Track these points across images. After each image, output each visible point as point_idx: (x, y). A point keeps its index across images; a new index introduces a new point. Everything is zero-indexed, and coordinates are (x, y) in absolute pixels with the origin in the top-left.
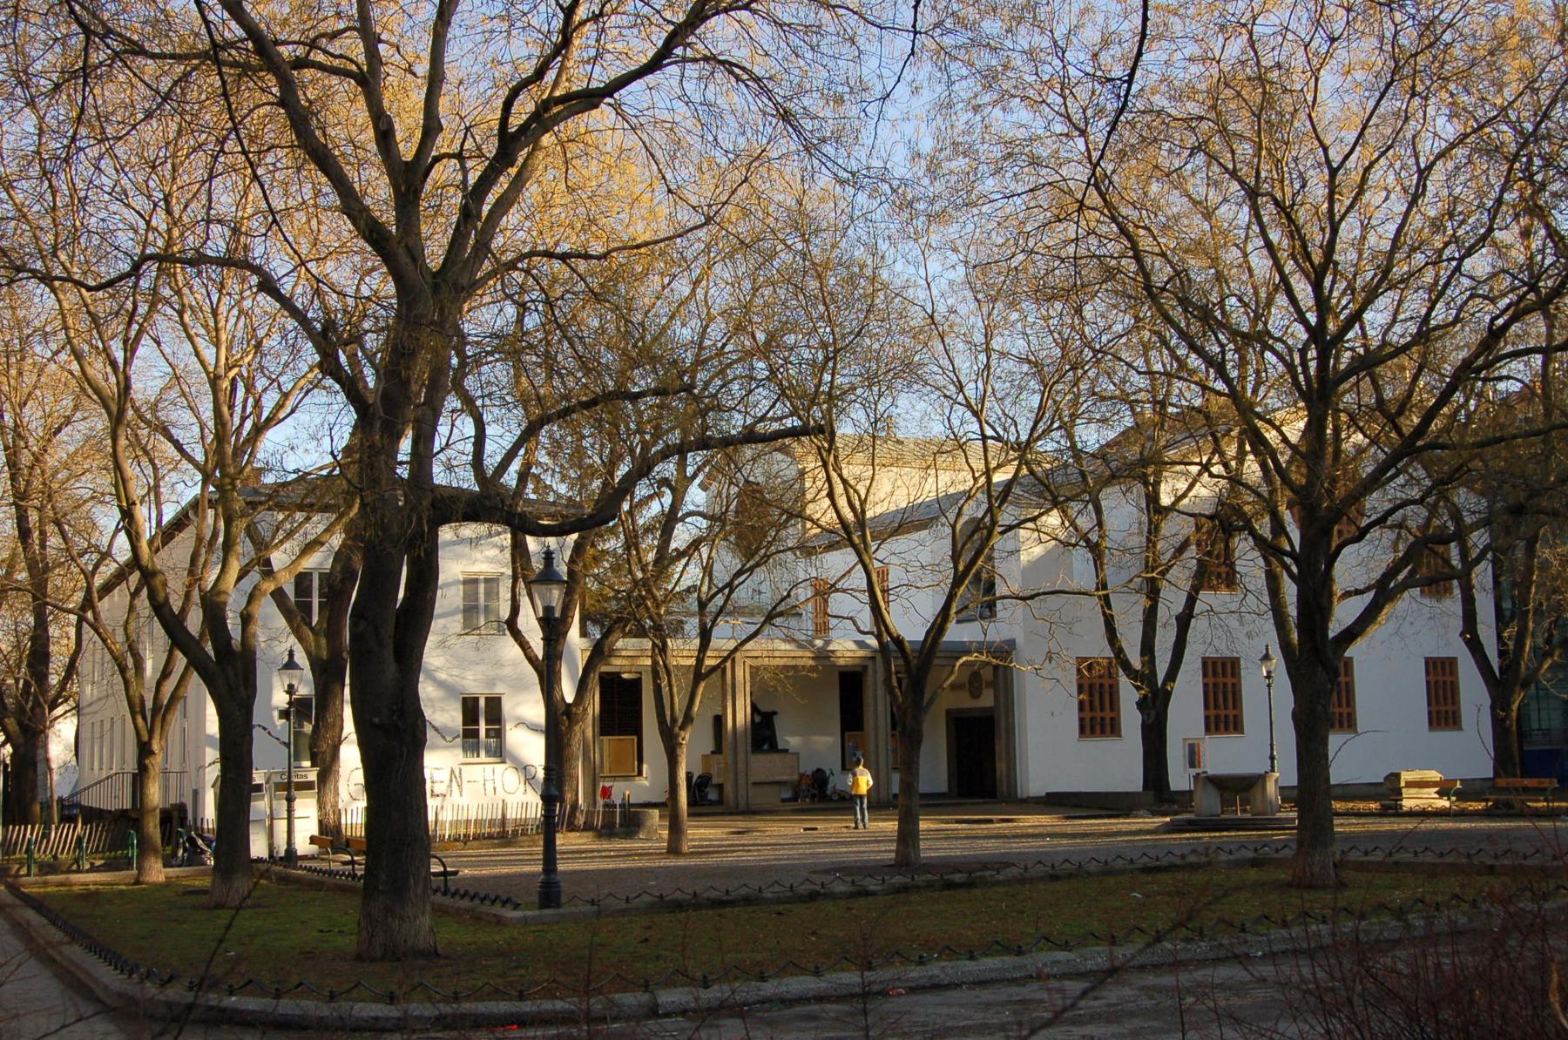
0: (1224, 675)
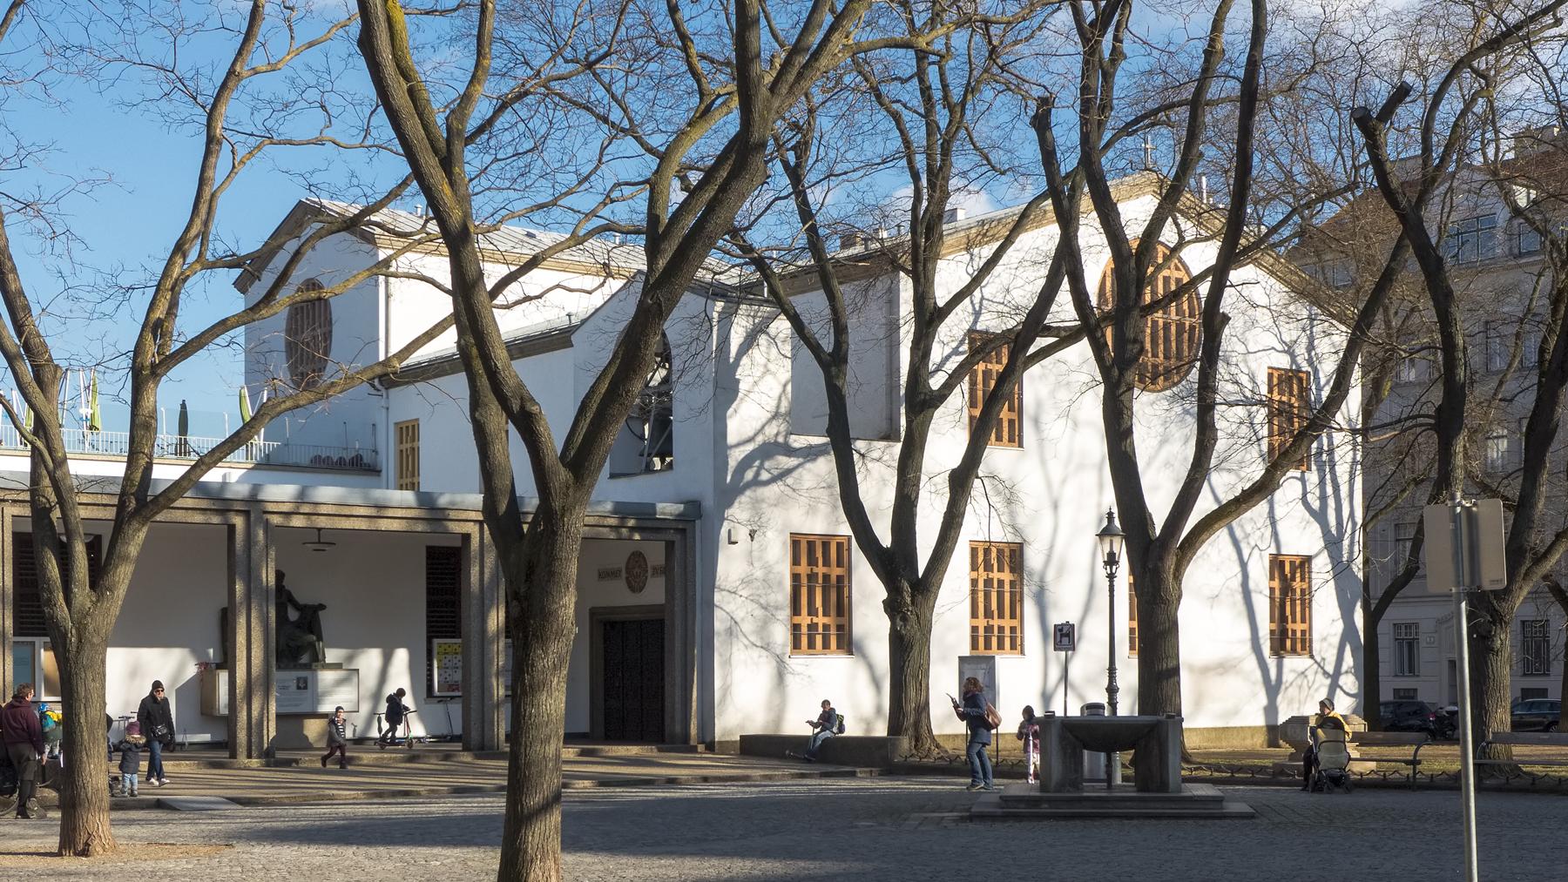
0: (1001, 616)
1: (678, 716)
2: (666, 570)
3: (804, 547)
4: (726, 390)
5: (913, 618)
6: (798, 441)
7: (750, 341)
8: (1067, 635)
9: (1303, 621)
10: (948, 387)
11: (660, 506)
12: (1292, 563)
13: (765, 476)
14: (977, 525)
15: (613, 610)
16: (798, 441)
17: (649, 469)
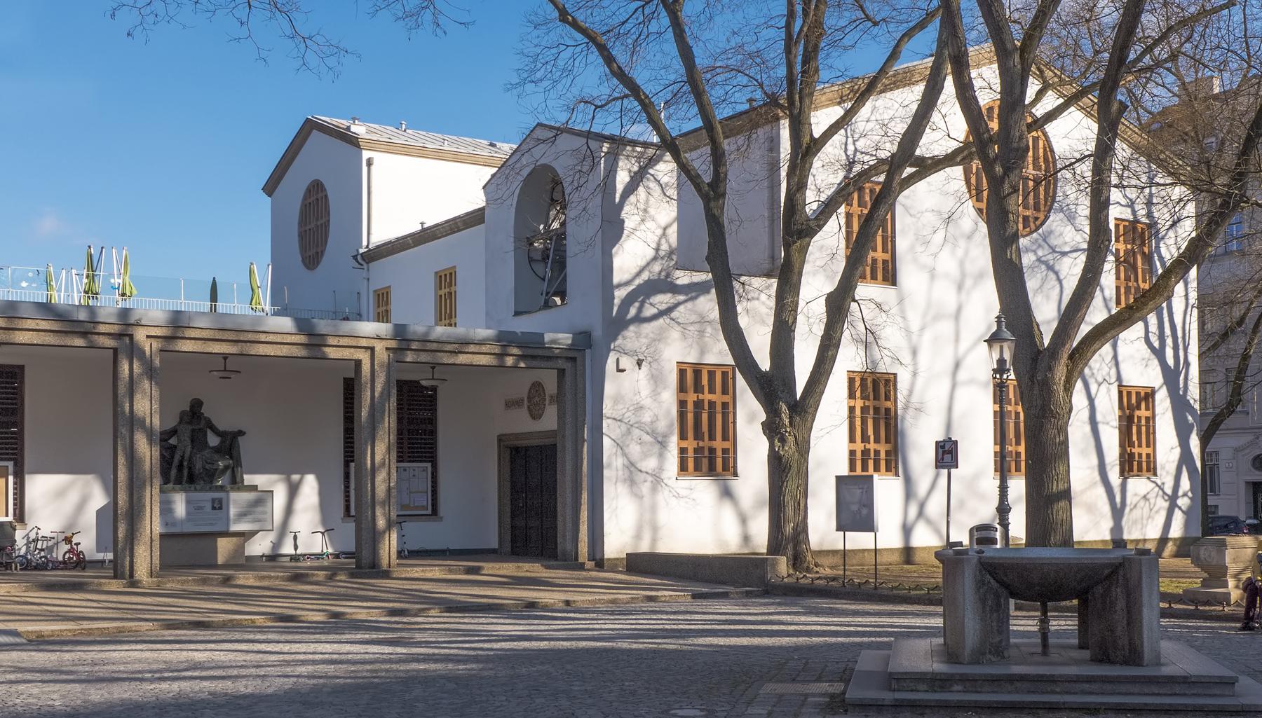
1: (569, 536)
2: (559, 399)
3: (692, 378)
4: (613, 229)
5: (791, 439)
6: (683, 278)
7: (637, 179)
8: (950, 452)
9: (1148, 446)
10: (828, 208)
11: (548, 337)
12: (1138, 393)
13: (649, 311)
14: (849, 359)
15: (516, 436)
16: (683, 278)
17: (547, 305)
